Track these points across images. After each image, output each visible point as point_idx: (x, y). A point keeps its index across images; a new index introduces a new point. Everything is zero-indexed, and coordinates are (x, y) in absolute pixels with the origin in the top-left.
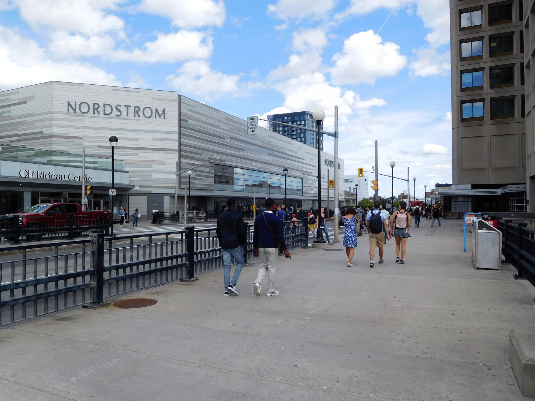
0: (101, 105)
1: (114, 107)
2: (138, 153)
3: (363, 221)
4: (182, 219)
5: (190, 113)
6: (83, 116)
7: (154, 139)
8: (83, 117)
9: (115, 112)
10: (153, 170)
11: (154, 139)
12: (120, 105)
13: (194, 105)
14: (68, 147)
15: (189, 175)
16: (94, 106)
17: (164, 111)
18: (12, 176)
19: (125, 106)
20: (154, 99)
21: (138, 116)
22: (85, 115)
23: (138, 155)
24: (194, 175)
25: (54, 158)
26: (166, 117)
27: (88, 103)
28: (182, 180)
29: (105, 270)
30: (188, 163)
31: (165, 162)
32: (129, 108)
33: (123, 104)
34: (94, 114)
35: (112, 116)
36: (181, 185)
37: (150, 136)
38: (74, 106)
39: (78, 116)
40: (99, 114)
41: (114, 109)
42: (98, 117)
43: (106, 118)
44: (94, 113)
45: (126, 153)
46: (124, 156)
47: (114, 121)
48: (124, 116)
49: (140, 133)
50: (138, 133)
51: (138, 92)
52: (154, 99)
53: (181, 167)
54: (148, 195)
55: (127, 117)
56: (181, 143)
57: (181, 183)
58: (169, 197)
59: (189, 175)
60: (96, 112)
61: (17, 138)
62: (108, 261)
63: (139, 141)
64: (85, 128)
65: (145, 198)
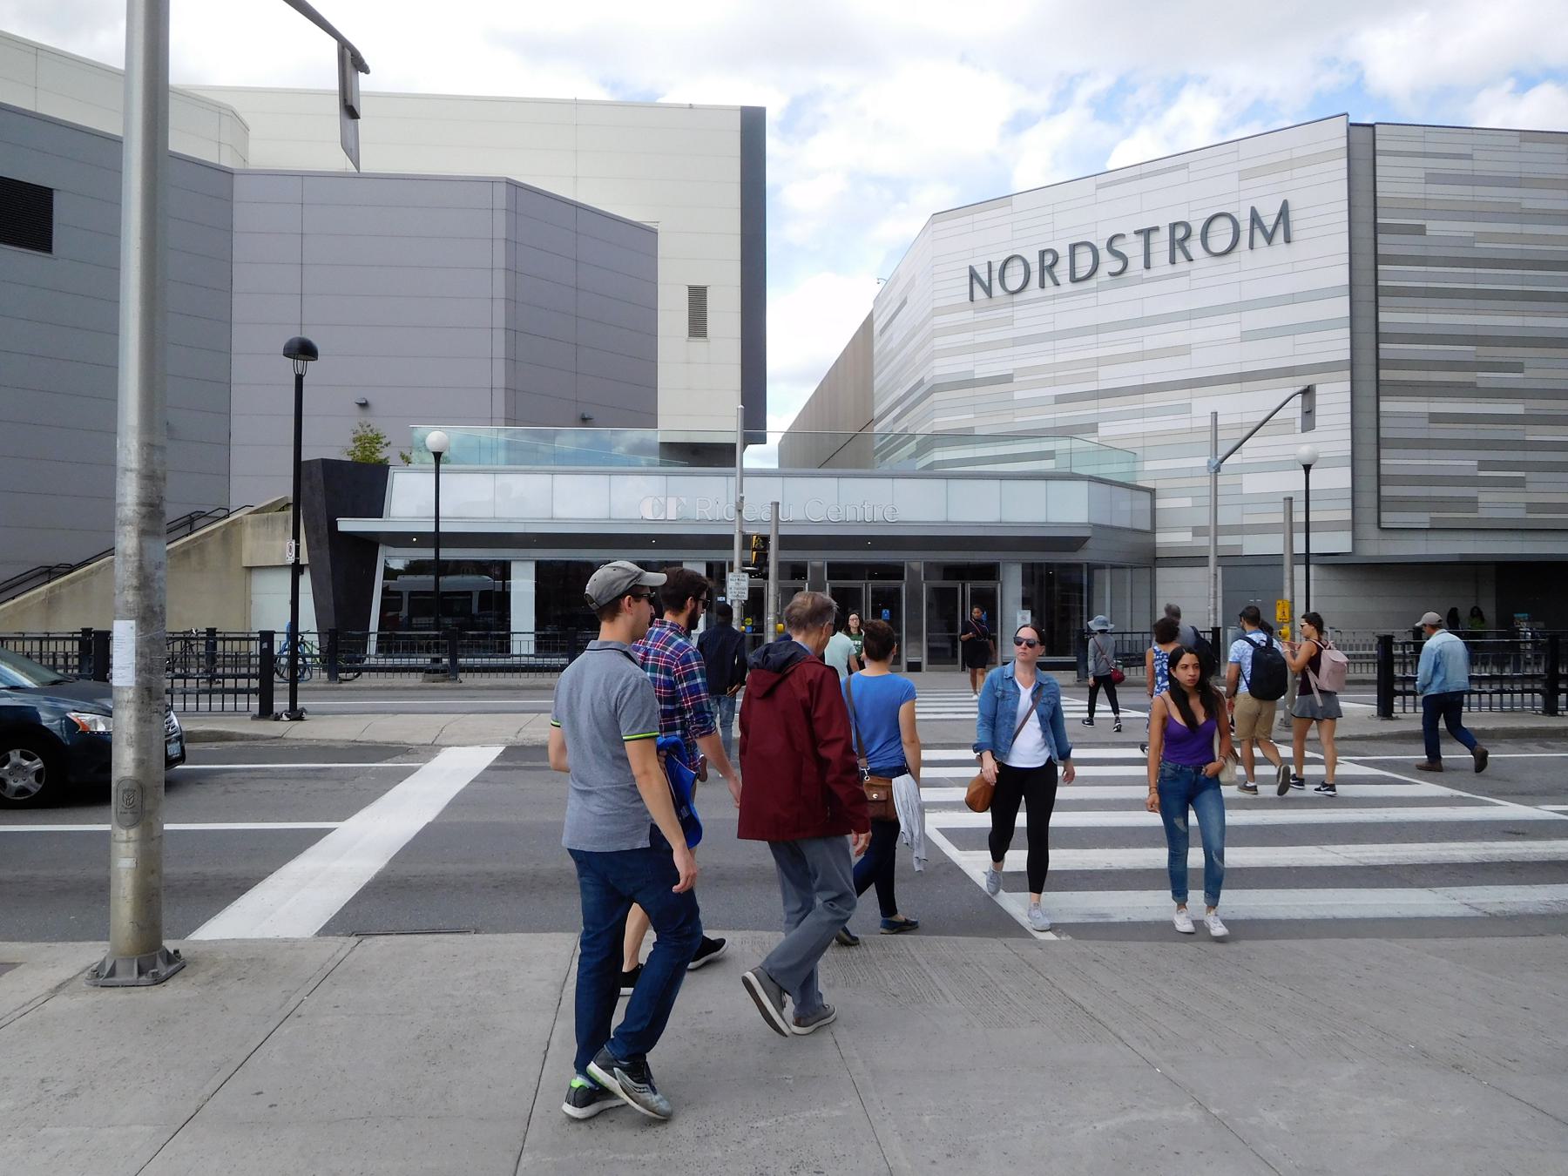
0: (1064, 252)
1: (1102, 246)
2: (1189, 401)
5: (1437, 191)
6: (1013, 304)
7: (1247, 336)
8: (1011, 309)
9: (1109, 264)
10: (1245, 461)
11: (1247, 336)
13: (1466, 150)
14: (972, 416)
15: (434, 453)
16: (1042, 260)
17: (1284, 213)
19: (1137, 233)
20: (1245, 175)
21: (1185, 259)
22: (1017, 298)
23: (1188, 408)
24: (1475, 463)
25: (939, 455)
26: (1295, 236)
28: (1386, 491)
30: (1431, 414)
32: (1154, 237)
33: (1128, 228)
34: (1043, 287)
35: (1099, 280)
36: (1384, 516)
37: (1229, 327)
38: (985, 278)
40: (1059, 285)
41: (1104, 255)
42: (1054, 297)
45: (1146, 406)
46: (1136, 421)
47: (1104, 296)
48: (1136, 273)
51: (1185, 166)
52: (1245, 175)
55: (1146, 274)
56: (1381, 329)
59: (434, 453)
60: (1179, 255)
61: (897, 411)
63: (1190, 354)
64: (1016, 342)
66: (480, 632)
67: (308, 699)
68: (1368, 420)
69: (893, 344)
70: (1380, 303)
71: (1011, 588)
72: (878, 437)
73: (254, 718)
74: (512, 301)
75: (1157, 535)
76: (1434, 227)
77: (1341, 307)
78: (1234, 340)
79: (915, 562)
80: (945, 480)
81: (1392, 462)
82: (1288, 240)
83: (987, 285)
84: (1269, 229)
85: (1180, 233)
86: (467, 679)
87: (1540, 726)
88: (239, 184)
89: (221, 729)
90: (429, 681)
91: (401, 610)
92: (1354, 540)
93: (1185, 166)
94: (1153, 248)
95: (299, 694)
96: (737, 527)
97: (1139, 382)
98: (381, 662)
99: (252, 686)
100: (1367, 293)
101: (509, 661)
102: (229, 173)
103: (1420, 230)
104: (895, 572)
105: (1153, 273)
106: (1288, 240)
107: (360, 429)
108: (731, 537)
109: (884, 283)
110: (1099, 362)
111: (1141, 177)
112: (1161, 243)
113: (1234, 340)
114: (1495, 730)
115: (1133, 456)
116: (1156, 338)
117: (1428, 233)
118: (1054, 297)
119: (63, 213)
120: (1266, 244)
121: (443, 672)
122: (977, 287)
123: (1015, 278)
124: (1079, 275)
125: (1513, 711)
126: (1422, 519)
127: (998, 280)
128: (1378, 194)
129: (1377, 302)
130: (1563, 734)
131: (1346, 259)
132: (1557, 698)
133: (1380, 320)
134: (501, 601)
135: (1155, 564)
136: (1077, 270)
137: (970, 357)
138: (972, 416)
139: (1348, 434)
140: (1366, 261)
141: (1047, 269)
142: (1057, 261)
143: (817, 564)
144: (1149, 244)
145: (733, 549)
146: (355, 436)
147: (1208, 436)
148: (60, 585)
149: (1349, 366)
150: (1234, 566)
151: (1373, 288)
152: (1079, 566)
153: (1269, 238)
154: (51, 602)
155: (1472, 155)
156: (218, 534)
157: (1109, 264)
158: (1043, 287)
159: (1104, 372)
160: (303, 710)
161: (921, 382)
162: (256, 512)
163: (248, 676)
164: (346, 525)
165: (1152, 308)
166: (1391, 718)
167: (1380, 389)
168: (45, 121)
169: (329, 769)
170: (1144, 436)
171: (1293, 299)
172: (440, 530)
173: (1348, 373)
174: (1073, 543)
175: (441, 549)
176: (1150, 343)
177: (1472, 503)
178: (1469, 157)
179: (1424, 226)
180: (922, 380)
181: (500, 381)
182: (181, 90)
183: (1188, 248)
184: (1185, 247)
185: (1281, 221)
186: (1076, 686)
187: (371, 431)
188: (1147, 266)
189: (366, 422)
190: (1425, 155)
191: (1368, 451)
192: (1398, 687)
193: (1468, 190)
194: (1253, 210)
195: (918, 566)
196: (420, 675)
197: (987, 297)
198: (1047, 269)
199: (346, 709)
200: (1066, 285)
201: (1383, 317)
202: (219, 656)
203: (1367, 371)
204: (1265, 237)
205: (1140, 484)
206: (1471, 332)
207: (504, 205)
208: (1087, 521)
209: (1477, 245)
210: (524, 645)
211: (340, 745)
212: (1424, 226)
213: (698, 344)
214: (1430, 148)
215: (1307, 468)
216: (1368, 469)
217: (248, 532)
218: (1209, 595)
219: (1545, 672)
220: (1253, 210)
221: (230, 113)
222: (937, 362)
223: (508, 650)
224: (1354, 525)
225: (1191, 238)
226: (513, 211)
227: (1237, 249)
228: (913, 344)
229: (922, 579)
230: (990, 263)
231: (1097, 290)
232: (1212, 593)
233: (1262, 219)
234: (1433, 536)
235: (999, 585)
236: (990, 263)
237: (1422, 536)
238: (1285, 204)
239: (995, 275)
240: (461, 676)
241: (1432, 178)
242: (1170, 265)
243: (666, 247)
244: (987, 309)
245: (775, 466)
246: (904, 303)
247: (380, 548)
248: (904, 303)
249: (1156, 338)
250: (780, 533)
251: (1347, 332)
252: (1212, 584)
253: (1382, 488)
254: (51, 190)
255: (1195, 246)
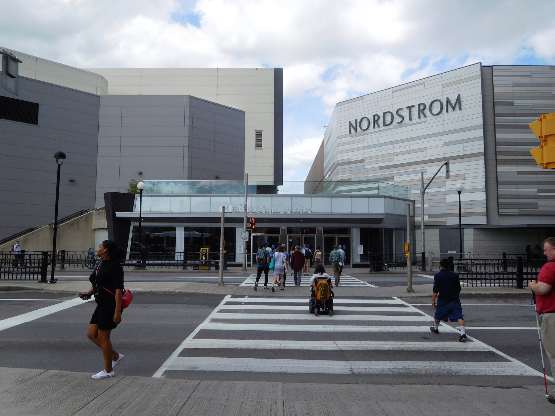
0: (381, 115)
1: (394, 113)
2: (426, 168)
3: (342, 267)
4: (432, 266)
6: (364, 134)
7: (447, 144)
9: (397, 119)
11: (447, 144)
12: (402, 109)
13: (529, 74)
14: (351, 174)
17: (459, 99)
18: (325, 212)
19: (407, 108)
20: (444, 86)
21: (424, 117)
22: (366, 132)
24: (537, 190)
25: (340, 189)
26: (463, 107)
27: (368, 118)
29: (41, 273)
31: (463, 175)
32: (413, 109)
35: (394, 125)
36: (500, 210)
37: (440, 141)
38: (354, 125)
39: (360, 135)
41: (396, 116)
42: (378, 131)
43: (387, 130)
44: (419, 117)
45: (411, 170)
47: (396, 131)
49: (428, 140)
50: (424, 140)
52: (444, 86)
53: (498, 180)
54: (441, 227)
55: (410, 122)
56: (497, 141)
57: (499, 206)
58: (438, 230)
60: (422, 115)
62: (57, 271)
64: (366, 148)
65: (437, 232)
66: (153, 252)
67: (58, 275)
68: (492, 175)
69: (328, 149)
70: (496, 131)
71: (355, 236)
72: (325, 183)
73: (39, 282)
74: (191, 137)
75: (416, 217)
76: (517, 103)
77: (480, 133)
78: (442, 146)
79: (320, 227)
80: (368, 198)
81: (503, 190)
82: (460, 109)
83: (355, 127)
84: (454, 105)
85: (422, 107)
86: (149, 268)
87: (509, 293)
88: (102, 101)
89: (23, 286)
90: (136, 269)
91: (163, 243)
92: (488, 219)
93: (423, 83)
94: (413, 113)
95: (55, 273)
96: (245, 214)
97: (408, 161)
98: (130, 262)
99: (514, 271)
100: (490, 127)
101: (173, 262)
102: (99, 97)
103: (512, 104)
104: (313, 230)
105: (413, 122)
106: (460, 109)
107: (132, 181)
108: (243, 218)
109: (326, 128)
110: (394, 154)
111: (408, 88)
112: (415, 111)
113: (442, 146)
114: (475, 294)
115: (407, 189)
116: (414, 145)
117: (514, 105)
118: (378, 131)
119: (42, 112)
120: (452, 110)
121: (140, 266)
122: (352, 129)
123: (365, 125)
124: (387, 123)
125: (508, 286)
126: (516, 211)
127: (359, 126)
128: (494, 91)
129: (495, 130)
130: (519, 296)
131: (481, 115)
132: (523, 282)
133: (496, 137)
134: (172, 242)
135: (415, 228)
136: (386, 122)
137: (349, 154)
138: (351, 174)
139: (484, 180)
140: (490, 115)
141: (376, 122)
142: (379, 118)
143: (284, 228)
144: (411, 112)
145: (243, 223)
146: (130, 184)
147: (420, 182)
148: (29, 235)
149: (484, 154)
150: (443, 228)
151: (494, 126)
152: (382, 229)
153: (454, 108)
154: (25, 241)
155: (531, 76)
156: (84, 218)
157: (397, 119)
158: (375, 128)
159: (396, 158)
160: (57, 280)
161: (334, 163)
162: (98, 210)
163: (38, 268)
164: (119, 214)
165: (412, 135)
166: (522, 288)
167: (497, 163)
168: (40, 82)
169: (34, 301)
170: (410, 181)
171: (462, 130)
172: (142, 216)
173: (483, 157)
174: (378, 220)
175: (141, 223)
176: (412, 147)
177: (536, 205)
178: (530, 76)
179: (513, 102)
180: (335, 162)
181: (186, 165)
182: (85, 70)
183: (425, 113)
184: (424, 112)
185: (458, 102)
186: (370, 274)
187: (136, 182)
188: (411, 119)
189: (133, 179)
190: (512, 76)
191: (493, 185)
192: (525, 276)
193: (530, 88)
194: (448, 98)
195: (321, 229)
196: (133, 267)
197: (355, 132)
198: (376, 122)
199: (157, 280)
200: (383, 127)
201: (497, 136)
202: (25, 259)
203: (492, 156)
204: (452, 108)
205: (409, 199)
206: (513, 141)
207: (188, 105)
208: (384, 212)
209: (534, 108)
210: (179, 257)
211: (55, 292)
212: (513, 102)
213: (259, 151)
214: (514, 74)
215: (459, 193)
216: (493, 192)
217: (94, 217)
218: (422, 240)
219: (517, 271)
220: (448, 98)
221: (101, 77)
222: (338, 155)
223: (174, 257)
224: (488, 213)
225: (426, 109)
226: (192, 107)
227: (442, 113)
228: (333, 149)
229: (322, 233)
230: (356, 120)
231: (393, 129)
232: (423, 239)
233: (451, 101)
234: (520, 218)
235: (351, 236)
236: (356, 120)
237: (516, 218)
238: (459, 96)
239: (358, 124)
240: (147, 267)
241: (515, 85)
242: (419, 119)
243: (248, 117)
244: (357, 136)
245: (302, 192)
246: (331, 134)
247: (131, 222)
248: (331, 134)
249: (414, 145)
250: (225, 216)
251: (482, 142)
252: (423, 236)
253: (499, 199)
254: (38, 104)
255: (427, 112)
